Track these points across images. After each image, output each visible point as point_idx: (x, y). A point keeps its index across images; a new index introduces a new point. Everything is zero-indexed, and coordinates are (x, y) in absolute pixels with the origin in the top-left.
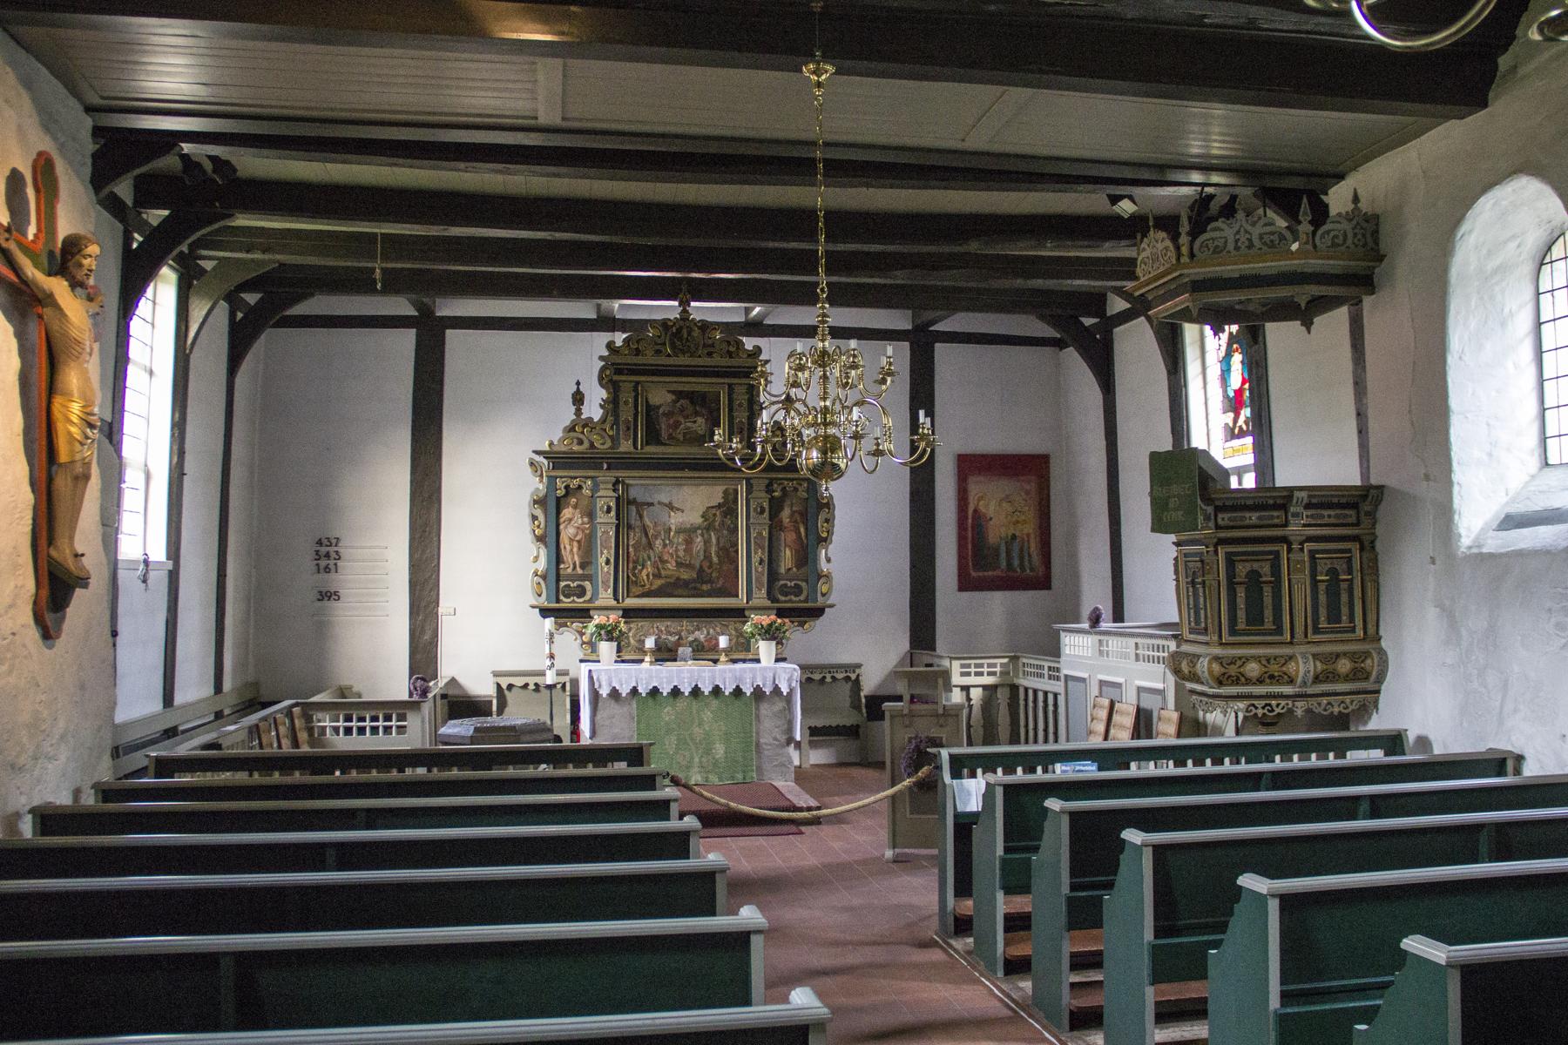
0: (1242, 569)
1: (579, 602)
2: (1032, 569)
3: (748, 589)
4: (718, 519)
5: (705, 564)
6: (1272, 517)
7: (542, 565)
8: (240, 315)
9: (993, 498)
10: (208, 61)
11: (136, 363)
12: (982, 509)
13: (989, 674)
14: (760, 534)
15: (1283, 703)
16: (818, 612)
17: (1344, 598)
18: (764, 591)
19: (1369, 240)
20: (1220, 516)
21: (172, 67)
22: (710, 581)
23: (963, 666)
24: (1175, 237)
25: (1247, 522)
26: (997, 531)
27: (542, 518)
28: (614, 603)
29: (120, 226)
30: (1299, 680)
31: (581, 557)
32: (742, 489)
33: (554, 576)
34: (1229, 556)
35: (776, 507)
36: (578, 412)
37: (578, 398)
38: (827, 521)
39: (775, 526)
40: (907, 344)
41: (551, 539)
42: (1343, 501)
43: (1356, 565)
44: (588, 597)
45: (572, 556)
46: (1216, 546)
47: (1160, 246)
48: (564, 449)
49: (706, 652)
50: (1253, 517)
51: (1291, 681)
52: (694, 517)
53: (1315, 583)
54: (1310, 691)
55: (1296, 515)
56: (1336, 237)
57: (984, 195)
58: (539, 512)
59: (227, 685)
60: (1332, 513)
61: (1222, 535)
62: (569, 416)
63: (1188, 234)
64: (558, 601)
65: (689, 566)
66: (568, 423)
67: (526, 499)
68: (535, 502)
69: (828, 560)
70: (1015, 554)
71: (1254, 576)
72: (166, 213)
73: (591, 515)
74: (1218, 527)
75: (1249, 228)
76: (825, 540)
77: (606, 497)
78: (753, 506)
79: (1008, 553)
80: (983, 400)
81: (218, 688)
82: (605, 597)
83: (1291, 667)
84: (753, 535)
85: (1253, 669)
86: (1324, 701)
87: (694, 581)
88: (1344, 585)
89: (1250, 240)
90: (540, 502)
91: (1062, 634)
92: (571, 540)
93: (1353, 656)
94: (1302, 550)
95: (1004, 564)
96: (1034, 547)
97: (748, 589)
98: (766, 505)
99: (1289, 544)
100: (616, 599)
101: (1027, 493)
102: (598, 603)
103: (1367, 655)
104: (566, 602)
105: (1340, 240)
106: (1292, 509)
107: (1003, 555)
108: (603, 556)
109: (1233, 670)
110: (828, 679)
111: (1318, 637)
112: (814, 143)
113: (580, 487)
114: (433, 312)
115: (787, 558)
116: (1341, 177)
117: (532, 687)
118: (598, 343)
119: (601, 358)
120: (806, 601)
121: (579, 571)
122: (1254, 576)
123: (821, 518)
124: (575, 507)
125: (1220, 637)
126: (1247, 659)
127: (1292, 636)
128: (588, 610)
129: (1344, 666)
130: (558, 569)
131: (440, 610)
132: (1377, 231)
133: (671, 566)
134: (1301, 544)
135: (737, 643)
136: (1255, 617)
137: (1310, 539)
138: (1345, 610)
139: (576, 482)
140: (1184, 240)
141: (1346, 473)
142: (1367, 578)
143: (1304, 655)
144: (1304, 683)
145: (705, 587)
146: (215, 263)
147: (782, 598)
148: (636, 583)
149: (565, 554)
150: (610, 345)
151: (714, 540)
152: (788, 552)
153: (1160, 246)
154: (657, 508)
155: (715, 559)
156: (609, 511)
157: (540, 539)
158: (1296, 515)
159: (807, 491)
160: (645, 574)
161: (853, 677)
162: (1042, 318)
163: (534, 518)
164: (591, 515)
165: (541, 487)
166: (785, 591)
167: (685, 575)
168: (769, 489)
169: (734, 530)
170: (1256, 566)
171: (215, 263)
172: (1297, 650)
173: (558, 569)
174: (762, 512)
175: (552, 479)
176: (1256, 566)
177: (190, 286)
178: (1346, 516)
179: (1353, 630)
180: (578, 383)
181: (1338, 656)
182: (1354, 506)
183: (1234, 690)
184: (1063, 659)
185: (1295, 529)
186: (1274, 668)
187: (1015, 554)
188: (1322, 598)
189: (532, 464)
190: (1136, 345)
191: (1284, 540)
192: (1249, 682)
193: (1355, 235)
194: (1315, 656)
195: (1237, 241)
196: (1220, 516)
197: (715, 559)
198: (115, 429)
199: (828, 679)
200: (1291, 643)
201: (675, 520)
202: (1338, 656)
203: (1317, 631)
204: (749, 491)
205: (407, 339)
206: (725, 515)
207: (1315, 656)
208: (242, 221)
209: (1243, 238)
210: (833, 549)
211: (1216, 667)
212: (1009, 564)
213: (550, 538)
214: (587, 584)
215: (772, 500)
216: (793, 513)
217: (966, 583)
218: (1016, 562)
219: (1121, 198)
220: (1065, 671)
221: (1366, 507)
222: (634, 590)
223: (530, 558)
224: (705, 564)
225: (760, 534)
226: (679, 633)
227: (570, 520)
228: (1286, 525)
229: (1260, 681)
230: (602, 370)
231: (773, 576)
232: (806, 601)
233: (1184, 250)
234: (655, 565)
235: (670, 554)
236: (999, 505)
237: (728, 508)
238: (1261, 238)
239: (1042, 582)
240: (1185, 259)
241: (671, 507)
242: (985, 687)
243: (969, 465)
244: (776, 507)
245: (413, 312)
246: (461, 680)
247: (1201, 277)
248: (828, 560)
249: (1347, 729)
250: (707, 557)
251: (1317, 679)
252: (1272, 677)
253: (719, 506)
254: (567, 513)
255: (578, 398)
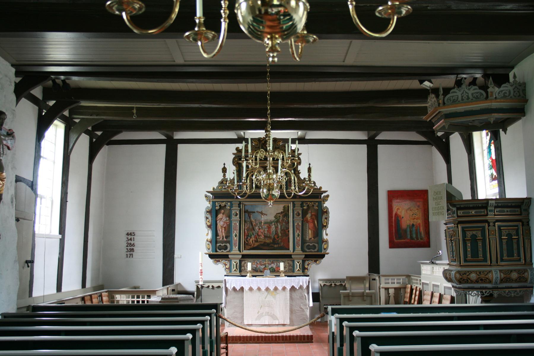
0: (469, 234)
1: (225, 252)
2: (421, 239)
3: (294, 248)
4: (281, 218)
5: (276, 237)
6: (482, 212)
7: (210, 237)
8: (94, 140)
9: (403, 208)
10: (72, 43)
11: (43, 158)
12: (399, 213)
13: (397, 283)
14: (298, 224)
15: (488, 291)
16: (322, 256)
17: (515, 246)
18: (300, 247)
19: (521, 93)
20: (459, 212)
21: (61, 48)
22: (278, 244)
23: (385, 280)
24: (437, 96)
25: (471, 214)
26: (405, 223)
27: (210, 218)
28: (238, 252)
29: (37, 108)
30: (494, 281)
31: (225, 234)
32: (291, 206)
33: (215, 241)
34: (463, 228)
35: (305, 213)
36: (224, 175)
37: (224, 170)
38: (326, 218)
39: (304, 221)
40: (366, 146)
41: (213, 227)
42: (513, 204)
43: (521, 232)
44: (228, 250)
45: (222, 233)
46: (457, 224)
47: (433, 100)
48: (218, 190)
49: (275, 272)
50: (473, 212)
51: (490, 282)
52: (271, 217)
53: (501, 240)
54: (500, 286)
55: (491, 211)
56: (505, 93)
57: (334, 83)
58: (209, 216)
59: (88, 285)
60: (509, 210)
61: (460, 219)
62: (220, 177)
63: (443, 94)
64: (216, 251)
65: (270, 237)
66: (220, 180)
67: (203, 210)
68: (207, 212)
69: (327, 235)
70: (414, 232)
71: (474, 237)
72: (54, 102)
73: (229, 216)
74: (458, 216)
75: (467, 91)
76: (325, 226)
77: (235, 210)
78: (295, 213)
79: (411, 232)
80: (403, 166)
81: (84, 285)
82: (235, 250)
83: (490, 275)
84: (296, 224)
85: (473, 276)
86: (507, 291)
87: (271, 243)
88: (515, 241)
89: (468, 96)
90: (209, 212)
91: (422, 265)
92: (222, 227)
93: (518, 271)
94: (494, 226)
95: (409, 237)
96: (422, 230)
97: (294, 248)
98: (300, 212)
99: (489, 223)
100: (240, 250)
101: (419, 206)
102: (232, 252)
103: (525, 271)
104: (220, 252)
105: (507, 94)
106: (489, 208)
107: (408, 233)
108: (235, 233)
109: (465, 277)
110: (333, 285)
111: (503, 263)
112: (266, 66)
113: (225, 206)
114: (172, 138)
115: (309, 234)
116: (512, 68)
117: (211, 287)
118: (232, 148)
119: (234, 154)
120: (318, 251)
121: (225, 239)
122: (474, 237)
123: (324, 217)
124: (223, 214)
125: (497, 262)
126: (471, 272)
127: (491, 262)
128: (228, 255)
129: (514, 275)
130: (216, 238)
131: (175, 256)
132: (525, 90)
133: (262, 237)
134: (494, 223)
135: (289, 269)
136: (475, 254)
137: (498, 221)
138: (515, 252)
139: (224, 204)
140: (441, 97)
141: (523, 194)
142: (525, 238)
143: (496, 271)
144: (496, 283)
145: (276, 246)
146: (79, 120)
147: (308, 250)
148: (247, 244)
149: (219, 232)
150: (237, 149)
151: (279, 227)
152: (310, 231)
153: (433, 100)
154: (256, 214)
155: (280, 235)
156: (236, 215)
157: (209, 227)
158: (491, 211)
159: (318, 206)
160: (252, 240)
161: (344, 284)
162: (419, 132)
163: (207, 218)
164: (229, 216)
165: (209, 205)
166: (309, 247)
167: (268, 241)
168: (302, 206)
169: (288, 222)
170: (474, 233)
171: (79, 120)
172: (492, 269)
173: (216, 238)
174: (299, 215)
175: (214, 203)
176: (474, 233)
177: (70, 129)
178: (515, 211)
179: (520, 260)
180: (224, 164)
181: (511, 271)
182: (519, 206)
183: (466, 285)
184: (422, 276)
185: (491, 217)
186: (482, 276)
187: (414, 232)
188: (505, 247)
189: (206, 196)
190: (456, 141)
191: (486, 221)
192: (472, 282)
193: (514, 92)
194: (501, 271)
195: (462, 97)
196: (459, 212)
197: (280, 235)
198: (34, 183)
199: (333, 285)
200: (490, 265)
201: (263, 219)
202: (511, 271)
203: (502, 260)
204: (294, 206)
205: (162, 148)
206: (284, 216)
207: (501, 271)
208: (84, 103)
209: (465, 96)
210: (328, 230)
211: (458, 275)
212: (411, 237)
213: (213, 226)
214: (228, 245)
215: (303, 210)
216: (312, 215)
217: (393, 245)
218: (414, 236)
219: (424, 81)
220: (422, 281)
221: (523, 207)
222: (247, 247)
223: (206, 234)
224: (276, 237)
225: (298, 224)
226: (265, 265)
227: (221, 219)
228: (487, 215)
229: (477, 282)
230: (234, 159)
231: (303, 241)
232: (318, 251)
233: (441, 101)
234: (255, 237)
235: (261, 231)
236: (406, 211)
237: (285, 213)
238: (472, 94)
239: (427, 244)
240: (441, 105)
241: (262, 213)
242: (395, 288)
243: (393, 195)
244: (305, 213)
245: (163, 137)
246: (183, 284)
247: (448, 112)
248: (327, 235)
249: (523, 302)
250: (277, 233)
251: (502, 281)
252: (482, 280)
253: (282, 213)
254: (220, 216)
255: (224, 170)
